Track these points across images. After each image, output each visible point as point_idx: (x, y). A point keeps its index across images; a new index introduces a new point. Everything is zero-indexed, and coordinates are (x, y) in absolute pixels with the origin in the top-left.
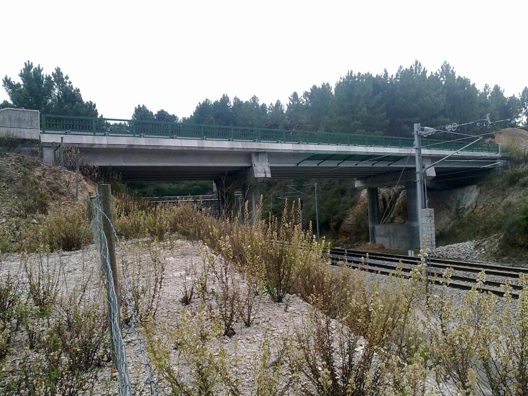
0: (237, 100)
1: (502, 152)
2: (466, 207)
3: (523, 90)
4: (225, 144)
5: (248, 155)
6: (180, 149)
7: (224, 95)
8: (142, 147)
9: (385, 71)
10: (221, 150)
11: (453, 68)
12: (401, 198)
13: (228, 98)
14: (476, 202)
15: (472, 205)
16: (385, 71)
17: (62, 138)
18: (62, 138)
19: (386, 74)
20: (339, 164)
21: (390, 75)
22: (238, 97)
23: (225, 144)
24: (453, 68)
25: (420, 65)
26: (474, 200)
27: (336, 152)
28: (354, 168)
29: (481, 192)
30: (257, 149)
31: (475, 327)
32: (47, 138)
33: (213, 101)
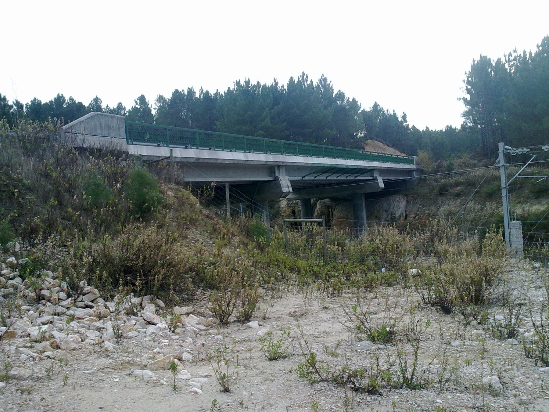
0: (71, 99)
1: (417, 164)
2: (397, 215)
3: (373, 105)
4: (239, 156)
5: (271, 168)
6: (232, 162)
7: (59, 94)
8: (241, 162)
9: (275, 80)
10: (259, 163)
11: (331, 82)
12: (319, 209)
13: (64, 98)
14: (406, 211)
15: (402, 214)
16: (275, 80)
17: (171, 150)
18: (171, 150)
19: (277, 84)
20: (328, 177)
21: (279, 86)
22: (73, 97)
23: (239, 156)
24: (331, 82)
25: (307, 77)
26: (404, 209)
27: (329, 166)
28: (335, 180)
29: (408, 202)
30: (283, 162)
31: (24, 363)
32: (135, 149)
33: (411, 122)
